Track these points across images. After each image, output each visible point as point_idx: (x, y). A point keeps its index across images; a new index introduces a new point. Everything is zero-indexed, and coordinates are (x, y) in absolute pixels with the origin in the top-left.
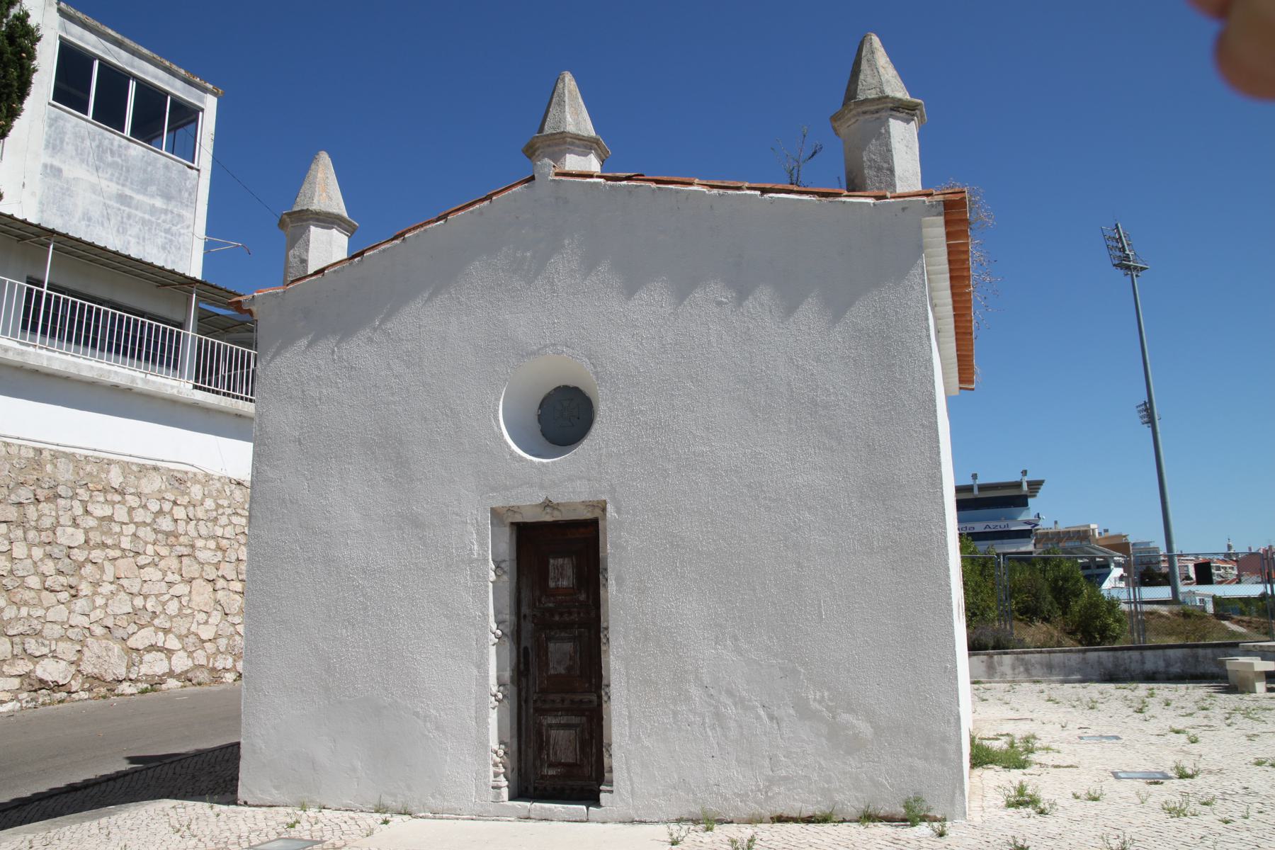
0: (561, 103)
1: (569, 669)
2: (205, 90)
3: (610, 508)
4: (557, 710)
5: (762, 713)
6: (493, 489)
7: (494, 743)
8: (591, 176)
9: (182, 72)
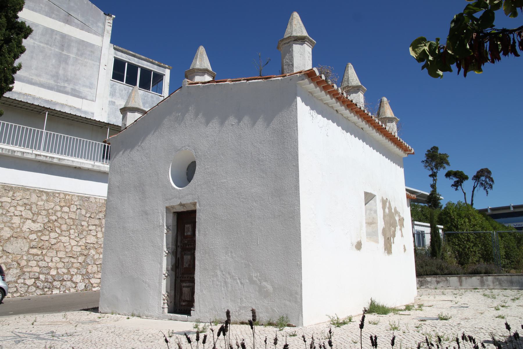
0: (196, 58)
2: (165, 68)
3: (197, 204)
5: (238, 281)
6: (167, 200)
8: (198, 83)
9: (157, 62)
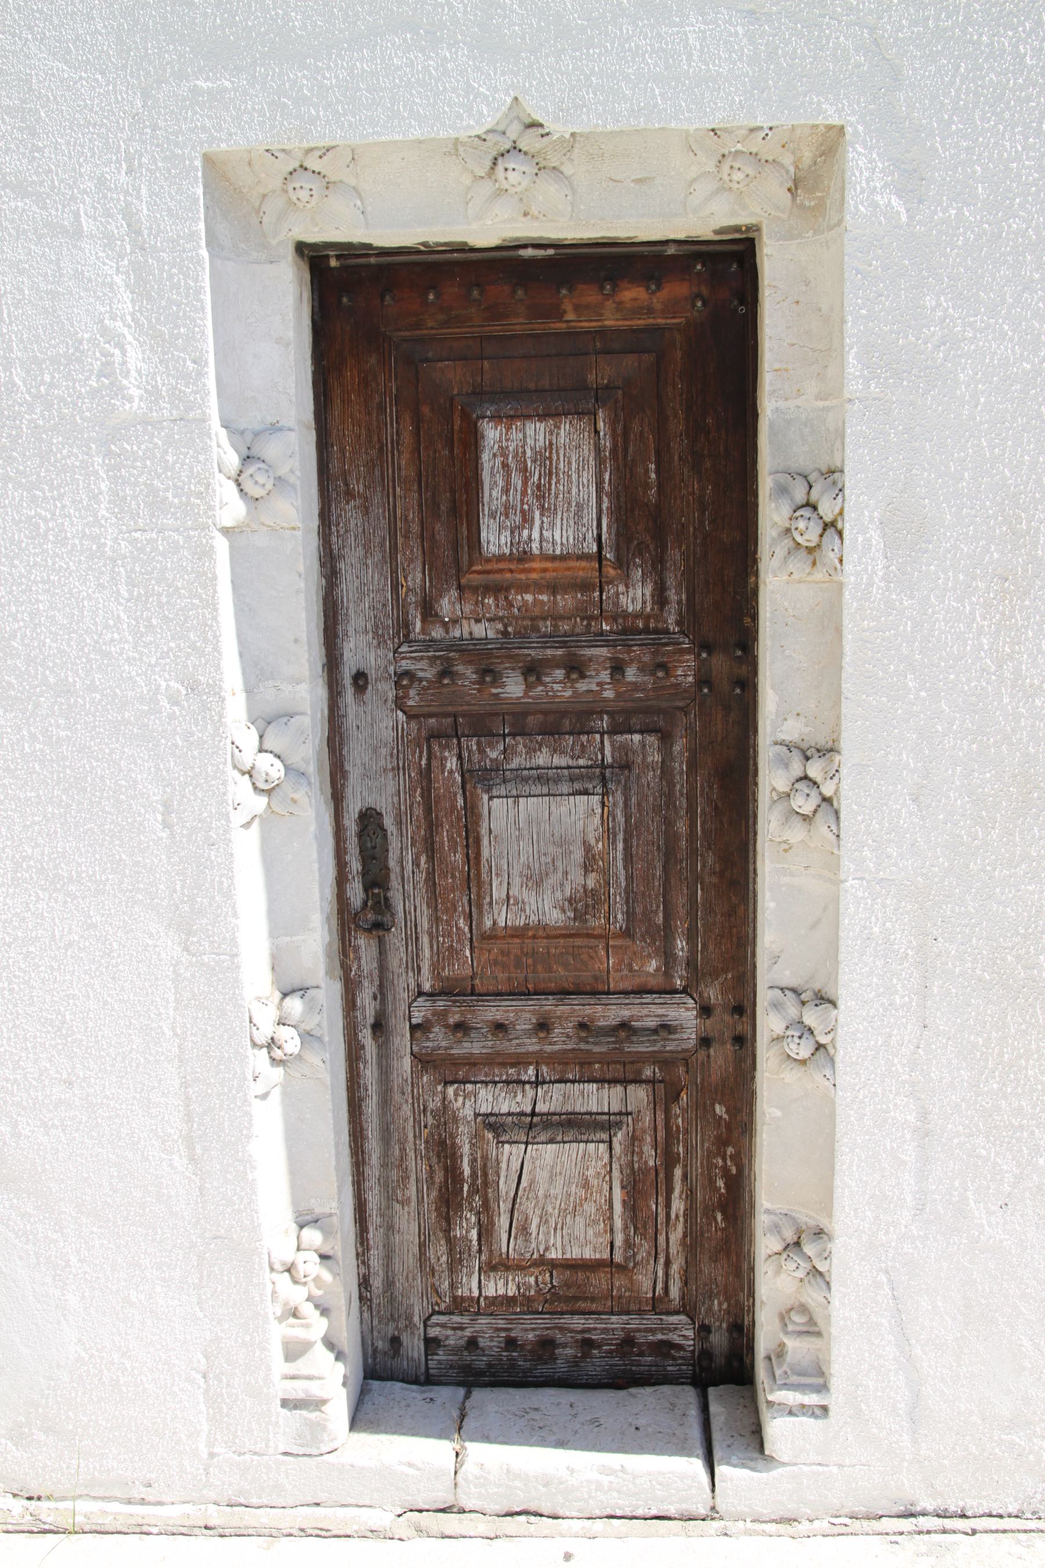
1: (584, 904)
3: (863, 168)
4: (519, 1061)
7: (277, 1234)
